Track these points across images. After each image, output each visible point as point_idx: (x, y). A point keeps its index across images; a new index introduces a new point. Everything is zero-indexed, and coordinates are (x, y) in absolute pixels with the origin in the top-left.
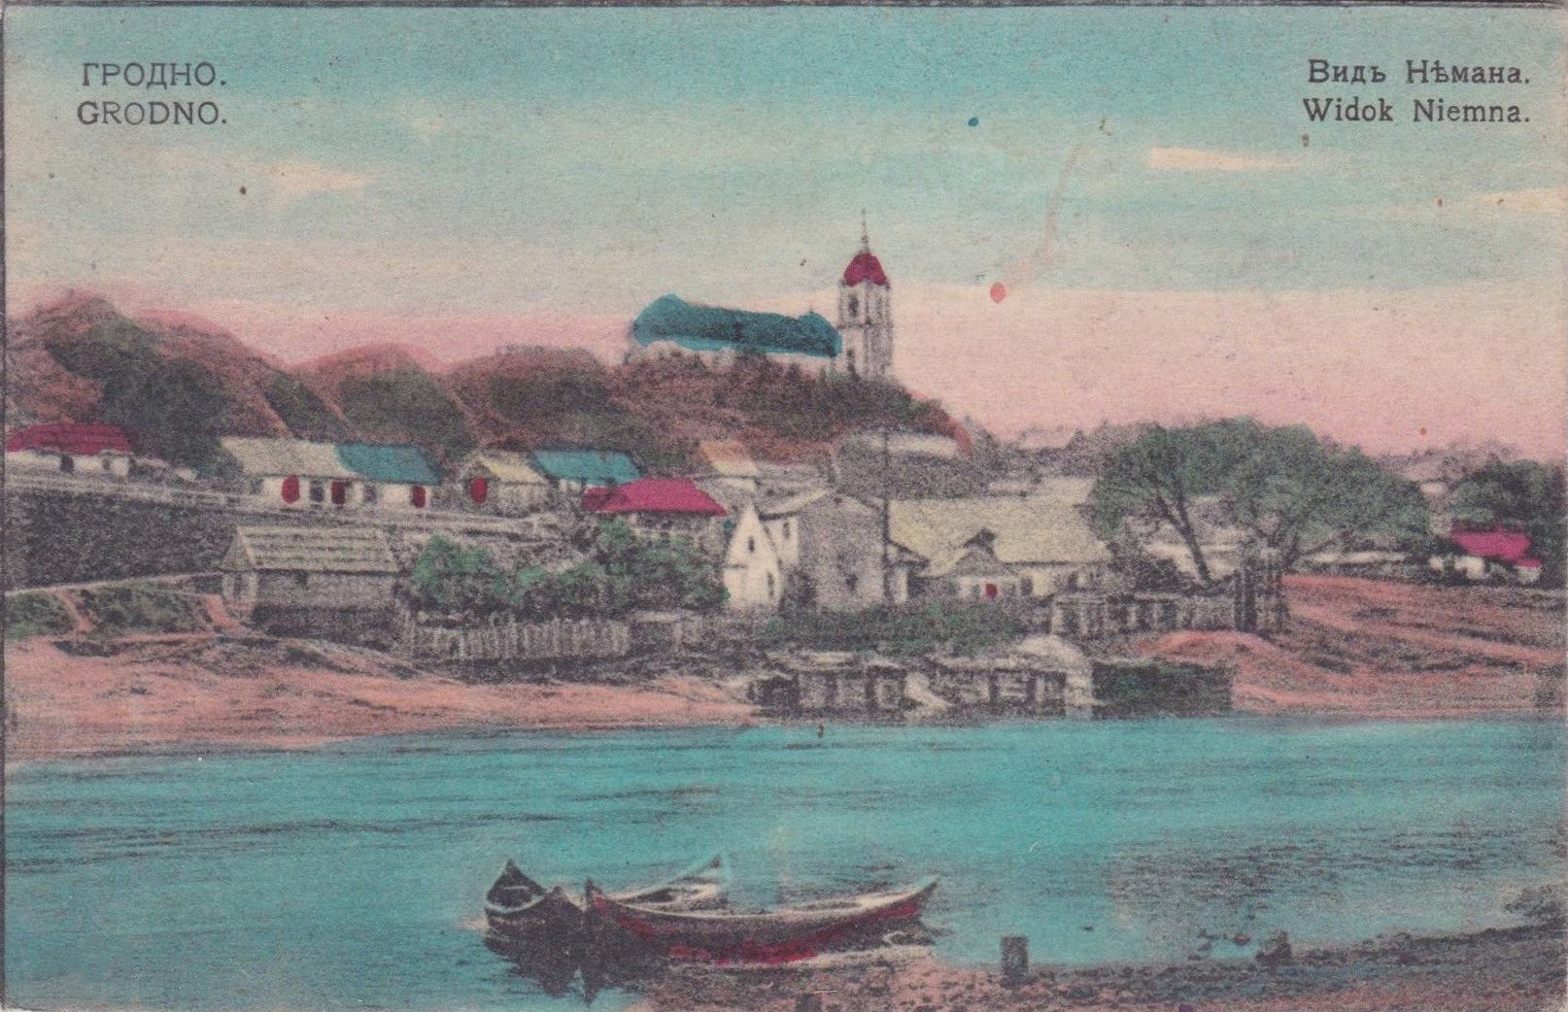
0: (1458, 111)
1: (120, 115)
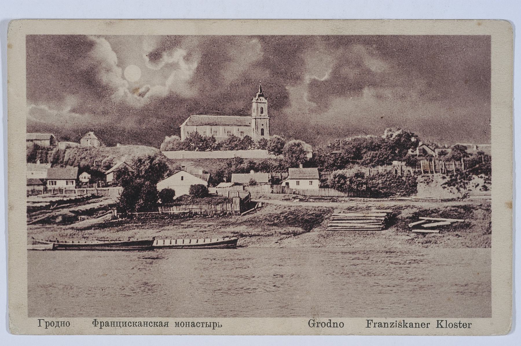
0: (425, 325)
1: (454, 326)
